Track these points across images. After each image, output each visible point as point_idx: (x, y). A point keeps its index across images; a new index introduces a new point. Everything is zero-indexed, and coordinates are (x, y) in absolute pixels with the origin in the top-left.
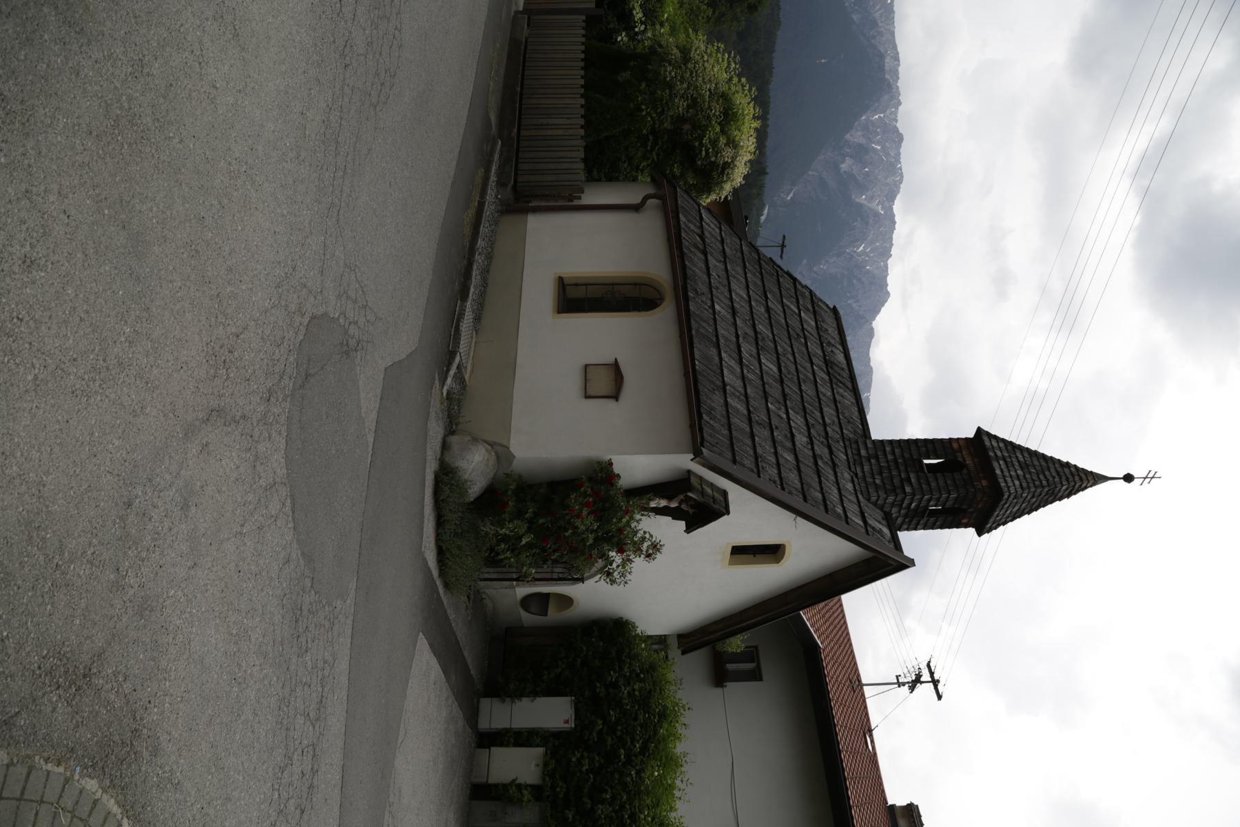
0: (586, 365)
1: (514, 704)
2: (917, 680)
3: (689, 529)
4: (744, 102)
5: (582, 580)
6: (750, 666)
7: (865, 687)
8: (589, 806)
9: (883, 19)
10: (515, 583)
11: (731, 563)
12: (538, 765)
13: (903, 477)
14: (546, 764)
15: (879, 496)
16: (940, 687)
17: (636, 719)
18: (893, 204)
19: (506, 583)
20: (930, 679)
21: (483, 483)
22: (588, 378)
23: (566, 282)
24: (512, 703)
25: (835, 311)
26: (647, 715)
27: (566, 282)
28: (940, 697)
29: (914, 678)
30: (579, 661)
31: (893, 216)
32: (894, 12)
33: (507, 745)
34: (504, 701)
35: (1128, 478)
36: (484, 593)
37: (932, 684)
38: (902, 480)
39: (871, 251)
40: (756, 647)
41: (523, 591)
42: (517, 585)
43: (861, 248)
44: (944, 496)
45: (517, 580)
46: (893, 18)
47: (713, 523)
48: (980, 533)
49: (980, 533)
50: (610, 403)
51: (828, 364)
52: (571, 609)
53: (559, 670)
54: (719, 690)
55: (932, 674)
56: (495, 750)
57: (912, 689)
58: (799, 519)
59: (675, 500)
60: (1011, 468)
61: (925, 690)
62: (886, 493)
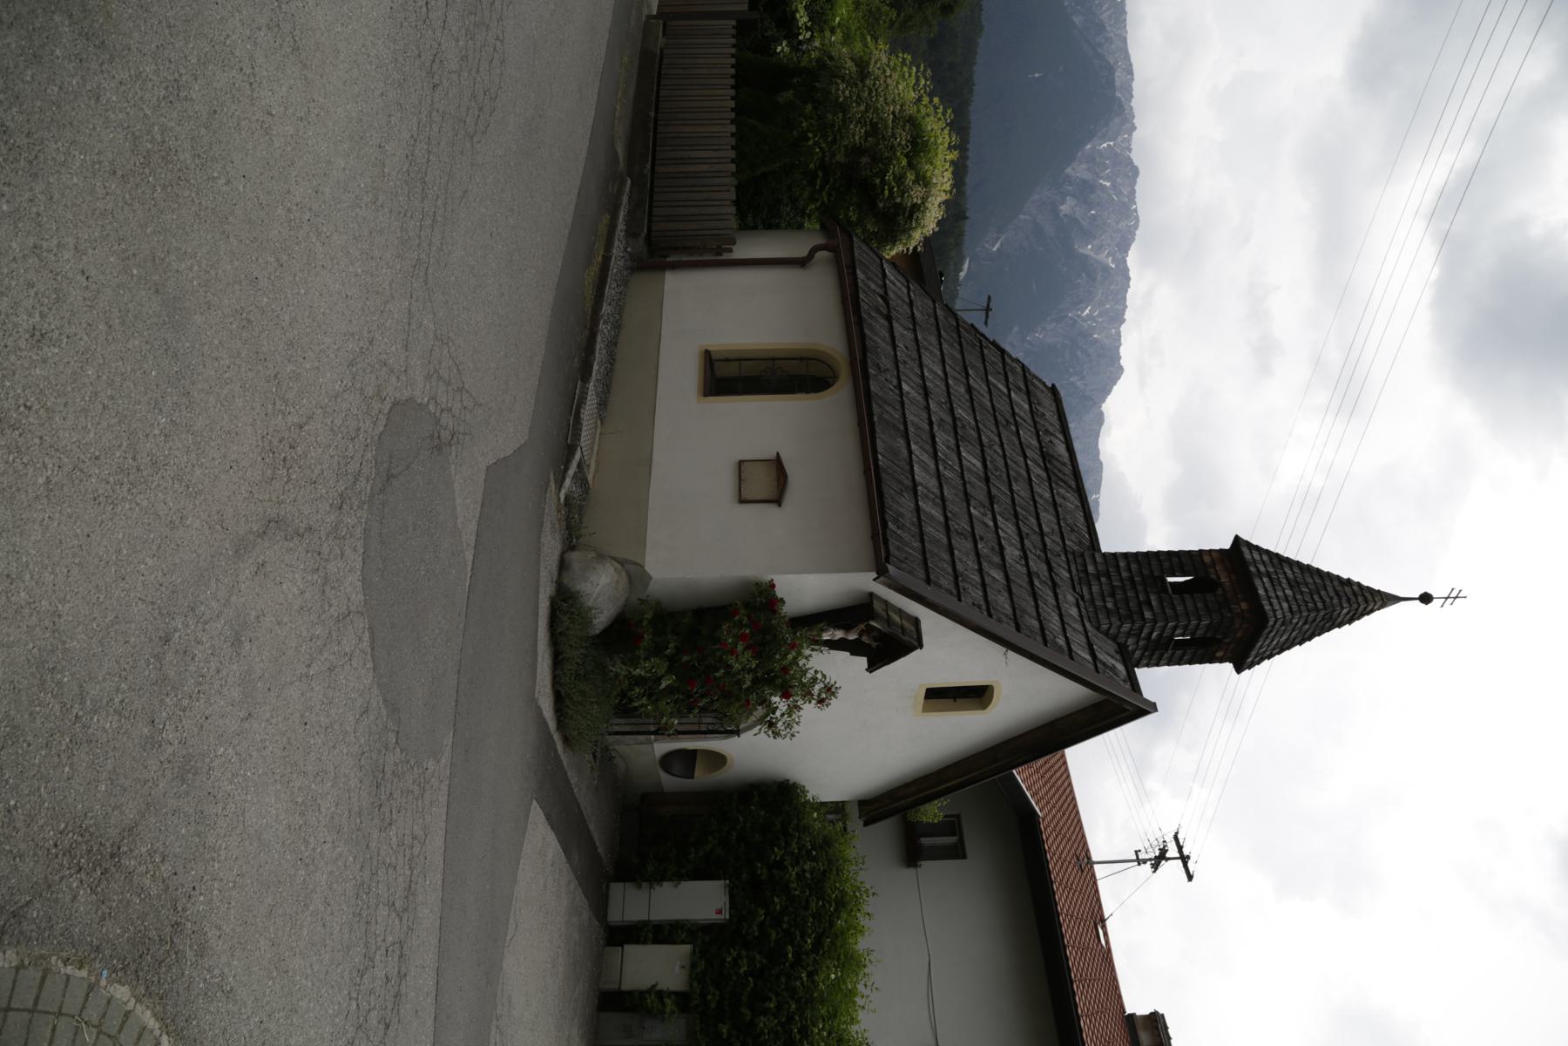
1: (652, 890)
2: (1162, 856)
3: (872, 667)
4: (936, 127)
5: (737, 733)
6: (950, 840)
7: (1096, 866)
8: (748, 1018)
9: (1112, 22)
10: (653, 737)
11: (926, 709)
12: (683, 967)
13: (1141, 599)
14: (693, 966)
16: (1190, 865)
17: (807, 908)
18: (1127, 256)
19: (642, 738)
20: (1178, 855)
21: (612, 611)
22: (742, 477)
23: (714, 356)
24: (651, 887)
25: (1054, 390)
26: (821, 903)
27: (713, 357)
28: (1190, 877)
29: (1157, 854)
30: (734, 835)
31: (1127, 270)
32: (1126, 13)
33: (645, 943)
34: (639, 887)
35: (1426, 598)
36: (614, 750)
37: (1180, 861)
38: (1140, 604)
39: (1100, 315)
40: (958, 817)
41: (662, 747)
42: (656, 740)
43: (1087, 311)
44: (1194, 623)
45: (655, 733)
46: (1125, 20)
47: (902, 659)
49: (1239, 670)
50: (771, 509)
51: (1046, 457)
54: (912, 870)
55: (1180, 848)
56: (630, 949)
57: (1155, 867)
58: (1010, 653)
59: (854, 630)
60: (1278, 587)
61: (1172, 868)
62: (1120, 619)
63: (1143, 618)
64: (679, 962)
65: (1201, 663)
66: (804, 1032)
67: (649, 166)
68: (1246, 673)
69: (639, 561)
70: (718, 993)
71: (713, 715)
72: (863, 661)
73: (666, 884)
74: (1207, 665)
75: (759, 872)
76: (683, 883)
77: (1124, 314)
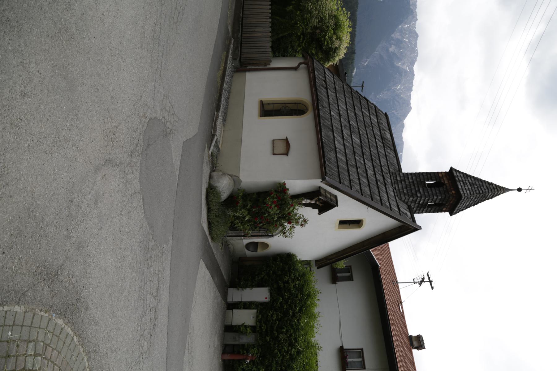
0: (273, 140)
2: (423, 281)
3: (320, 213)
5: (272, 236)
6: (348, 274)
7: (399, 284)
8: (276, 335)
14: (257, 317)
15: (405, 198)
16: (432, 284)
19: (239, 238)
20: (428, 281)
23: (264, 103)
26: (302, 295)
28: (432, 288)
31: (413, 72)
33: (240, 309)
34: (238, 290)
35: (520, 190)
36: (229, 242)
37: (429, 283)
39: (403, 88)
40: (350, 266)
41: (246, 241)
42: (244, 239)
44: (435, 198)
48: (451, 215)
49: (451, 215)
50: (285, 156)
52: (268, 248)
53: (262, 276)
54: (334, 285)
55: (429, 278)
57: (420, 284)
60: (466, 185)
61: (426, 285)
62: (409, 197)
63: (417, 196)
64: (252, 316)
65: (437, 212)
66: (296, 340)
67: (240, 34)
68: (454, 216)
69: (237, 175)
70: (266, 326)
71: (264, 230)
72: (317, 211)
73: (248, 289)
74: (440, 213)
75: (280, 285)
76: (253, 288)
77: (412, 88)
